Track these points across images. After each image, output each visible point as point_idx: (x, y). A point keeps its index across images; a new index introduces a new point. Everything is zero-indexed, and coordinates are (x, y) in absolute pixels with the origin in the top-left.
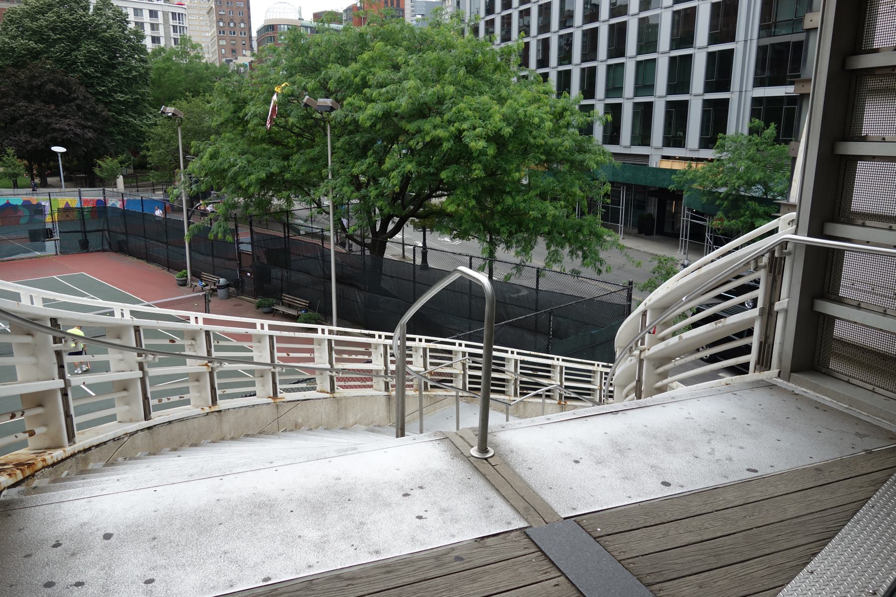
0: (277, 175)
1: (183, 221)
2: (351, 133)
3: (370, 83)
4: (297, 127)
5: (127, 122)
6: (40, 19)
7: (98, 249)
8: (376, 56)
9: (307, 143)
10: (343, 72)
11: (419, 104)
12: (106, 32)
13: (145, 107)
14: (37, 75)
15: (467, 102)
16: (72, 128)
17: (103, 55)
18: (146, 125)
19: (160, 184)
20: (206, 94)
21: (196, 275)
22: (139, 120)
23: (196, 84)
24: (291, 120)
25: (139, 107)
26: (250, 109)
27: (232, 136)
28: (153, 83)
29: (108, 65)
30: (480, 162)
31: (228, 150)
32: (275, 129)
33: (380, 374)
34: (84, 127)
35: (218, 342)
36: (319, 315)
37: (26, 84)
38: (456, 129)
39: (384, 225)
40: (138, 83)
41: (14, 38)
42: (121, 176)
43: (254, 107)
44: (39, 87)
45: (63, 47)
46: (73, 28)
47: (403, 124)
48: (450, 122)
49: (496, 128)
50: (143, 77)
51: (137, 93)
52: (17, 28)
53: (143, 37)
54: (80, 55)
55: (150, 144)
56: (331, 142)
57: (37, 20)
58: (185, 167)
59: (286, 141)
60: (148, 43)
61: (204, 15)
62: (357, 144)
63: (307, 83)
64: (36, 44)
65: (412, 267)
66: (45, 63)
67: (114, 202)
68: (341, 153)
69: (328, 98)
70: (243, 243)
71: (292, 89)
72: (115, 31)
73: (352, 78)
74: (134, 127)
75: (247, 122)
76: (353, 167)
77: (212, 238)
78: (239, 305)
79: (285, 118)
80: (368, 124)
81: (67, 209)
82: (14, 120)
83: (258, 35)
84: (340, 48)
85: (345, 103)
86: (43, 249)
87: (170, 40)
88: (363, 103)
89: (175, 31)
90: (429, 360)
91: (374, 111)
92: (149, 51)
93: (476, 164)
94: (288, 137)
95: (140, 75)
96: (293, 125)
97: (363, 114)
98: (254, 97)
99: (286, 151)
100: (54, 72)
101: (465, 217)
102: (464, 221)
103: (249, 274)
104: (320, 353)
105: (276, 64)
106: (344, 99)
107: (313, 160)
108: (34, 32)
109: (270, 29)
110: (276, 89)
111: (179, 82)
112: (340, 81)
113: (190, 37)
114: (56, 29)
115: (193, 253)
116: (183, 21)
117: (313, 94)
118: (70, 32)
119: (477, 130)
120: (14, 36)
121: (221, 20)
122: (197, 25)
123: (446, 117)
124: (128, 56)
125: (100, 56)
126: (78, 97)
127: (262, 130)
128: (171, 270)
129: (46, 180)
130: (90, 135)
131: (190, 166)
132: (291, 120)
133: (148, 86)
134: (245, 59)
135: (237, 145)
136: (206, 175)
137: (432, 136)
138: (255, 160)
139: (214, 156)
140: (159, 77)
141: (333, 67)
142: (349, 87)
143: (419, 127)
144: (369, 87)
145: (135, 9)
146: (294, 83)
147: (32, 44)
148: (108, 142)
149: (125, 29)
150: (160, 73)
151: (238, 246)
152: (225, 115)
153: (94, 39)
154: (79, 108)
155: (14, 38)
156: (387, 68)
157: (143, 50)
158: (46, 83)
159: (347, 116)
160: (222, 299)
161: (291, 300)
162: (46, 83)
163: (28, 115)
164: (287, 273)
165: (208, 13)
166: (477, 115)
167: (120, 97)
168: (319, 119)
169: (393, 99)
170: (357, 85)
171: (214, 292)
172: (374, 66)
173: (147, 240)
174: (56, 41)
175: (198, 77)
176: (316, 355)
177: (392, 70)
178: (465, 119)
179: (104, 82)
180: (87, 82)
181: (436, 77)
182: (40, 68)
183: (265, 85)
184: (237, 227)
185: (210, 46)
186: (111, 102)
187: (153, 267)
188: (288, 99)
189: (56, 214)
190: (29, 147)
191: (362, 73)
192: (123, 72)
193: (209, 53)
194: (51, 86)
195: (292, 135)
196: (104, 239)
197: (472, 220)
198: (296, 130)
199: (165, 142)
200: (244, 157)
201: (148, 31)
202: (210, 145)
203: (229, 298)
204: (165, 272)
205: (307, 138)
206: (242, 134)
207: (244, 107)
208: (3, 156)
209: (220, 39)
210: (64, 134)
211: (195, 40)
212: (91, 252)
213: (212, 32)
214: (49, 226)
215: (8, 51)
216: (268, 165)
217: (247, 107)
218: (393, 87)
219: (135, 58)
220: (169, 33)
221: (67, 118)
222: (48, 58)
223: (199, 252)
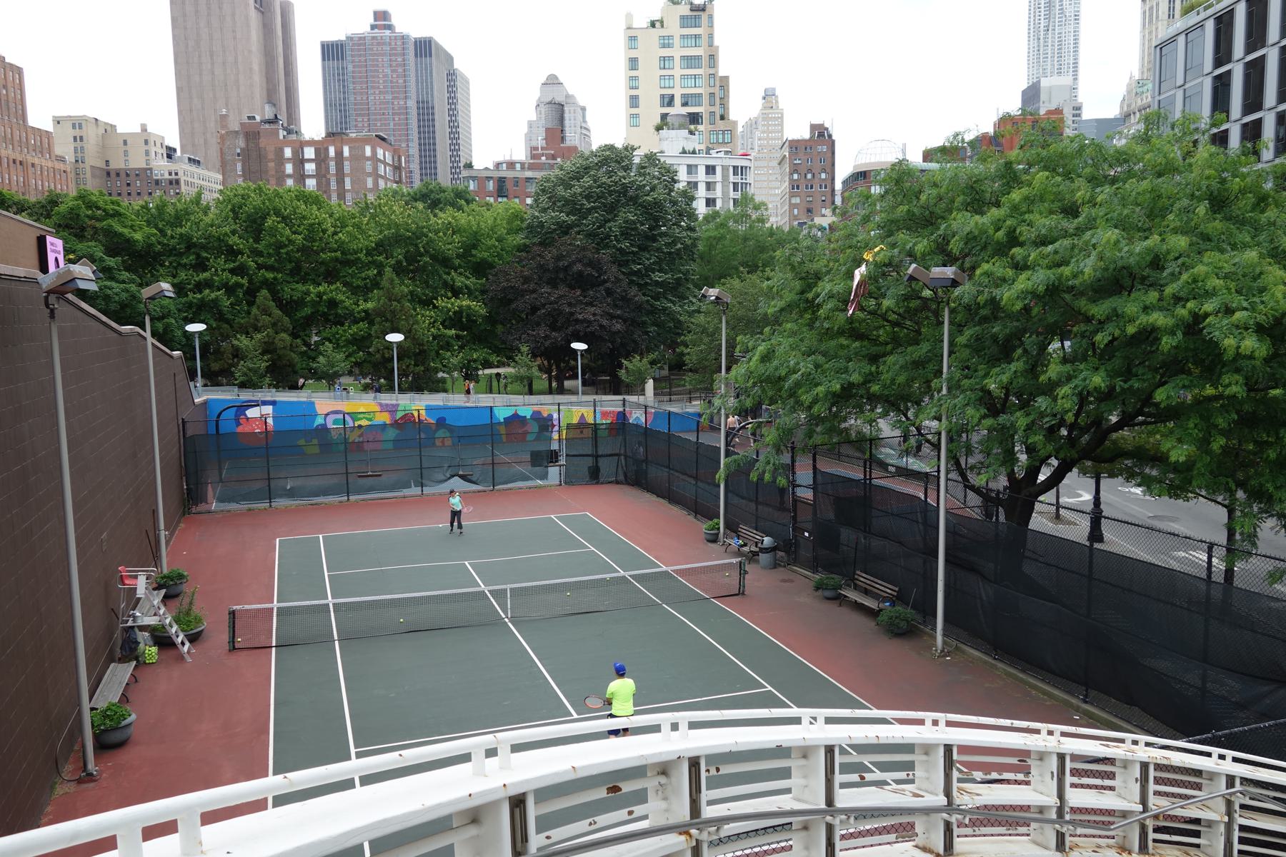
0: (859, 385)
1: (720, 448)
2: (985, 319)
3: (1022, 239)
4: (893, 312)
5: (665, 309)
6: (574, 186)
7: (610, 480)
8: (1035, 195)
9: (907, 335)
10: (977, 223)
11: (1114, 270)
12: (648, 195)
13: (688, 288)
14: (564, 253)
15: (1211, 263)
16: (598, 318)
17: (643, 224)
18: (687, 312)
19: (697, 390)
20: (767, 269)
21: (732, 527)
22: (680, 306)
23: (756, 256)
24: (887, 303)
25: (681, 289)
26: (825, 287)
27: (796, 328)
28: (702, 258)
29: (647, 237)
30: (1238, 371)
31: (788, 348)
32: (860, 314)
33: (1047, 816)
34: (612, 317)
35: (718, 770)
36: (913, 612)
37: (551, 266)
38: (1190, 312)
39: (1033, 471)
40: (681, 258)
41: (544, 210)
42: (651, 381)
43: (831, 284)
44: (566, 269)
45: (597, 217)
46: (610, 193)
47: (1082, 304)
48: (1178, 299)
49: (1276, 311)
50: (690, 249)
51: (680, 271)
52: (549, 198)
53: (693, 199)
54: (615, 227)
55: (689, 338)
56: (950, 335)
57: (571, 187)
58: (728, 369)
59: (875, 333)
60: (700, 208)
61: (774, 168)
62: (995, 338)
63: (915, 244)
64: (567, 216)
65: (1087, 551)
66: (575, 239)
67: (636, 416)
68: (966, 353)
69: (945, 265)
70: (801, 486)
71: (890, 254)
72: (660, 194)
73: (991, 232)
74: (671, 316)
75: (819, 306)
76: (986, 375)
77: (755, 479)
78: (791, 581)
79: (876, 298)
80: (1019, 306)
81: (582, 425)
82: (534, 309)
83: (843, 187)
84: (972, 187)
85: (978, 272)
86: (544, 476)
87: (729, 202)
88: (1010, 273)
89: (735, 189)
90: (1152, 787)
91: (1030, 283)
92: (701, 217)
93: (1228, 375)
94: (878, 328)
95: (686, 247)
96: (889, 309)
97: (1009, 289)
98: (831, 269)
99: (874, 350)
100: (584, 249)
101: (1199, 465)
102: (1195, 472)
103: (806, 534)
104: (927, 771)
105: (866, 220)
106: (973, 268)
107: (918, 364)
108: (567, 202)
109: (861, 176)
110: (865, 257)
111: (734, 254)
112: (970, 238)
113: (753, 195)
114: (592, 197)
115: (730, 495)
116: (746, 175)
117: (924, 261)
118: (606, 199)
119: (1238, 315)
120: (545, 209)
121: (796, 171)
122: (765, 181)
123: (1169, 290)
124: (673, 225)
125: (638, 225)
126: (608, 278)
127: (841, 318)
128: (699, 516)
129: (563, 383)
130: (618, 326)
131: (733, 372)
132: (887, 303)
133: (695, 261)
134: (825, 219)
135: (802, 340)
136: (755, 384)
137: (1140, 324)
138: (827, 363)
139: (766, 358)
140: (710, 250)
141: (960, 216)
142: (984, 248)
143: (1115, 310)
144: (1021, 245)
145: (689, 166)
146: (893, 246)
147: (563, 216)
148: (639, 336)
149: (671, 190)
150: (711, 245)
151: (793, 490)
152: (789, 297)
153: (634, 205)
154: (609, 292)
155: (544, 210)
156: (1051, 212)
157: (692, 215)
158: (574, 263)
159: (980, 293)
160: (764, 568)
161: (868, 582)
162: (574, 263)
163: (550, 304)
164: (865, 539)
165: (779, 164)
166: (1232, 285)
167: (658, 277)
168: (928, 299)
169: (1067, 263)
170: (998, 243)
171: (754, 555)
172: (1031, 212)
173: (672, 472)
174: (589, 211)
175: (759, 246)
176: (919, 773)
177: (1062, 215)
178: (1209, 294)
179: (641, 259)
180: (622, 260)
181: (1143, 221)
182: (570, 245)
183: (849, 251)
184: (793, 461)
185: (779, 206)
186: (646, 283)
187: (676, 511)
188: (884, 269)
189: (564, 432)
190: (547, 343)
191: (1008, 223)
192: (665, 245)
193: (777, 216)
194: (578, 267)
195: (886, 323)
196: (620, 469)
197: (1211, 472)
198: (893, 317)
199: (708, 335)
200: (810, 358)
201: (702, 192)
202: (763, 341)
203: (775, 568)
204: (691, 518)
205: (908, 329)
206: (811, 325)
207: (816, 284)
208: (517, 356)
209: (792, 195)
210: (588, 327)
211: (758, 199)
212: (602, 483)
213: (783, 188)
214: (555, 446)
215: (537, 226)
216: (846, 371)
217: (820, 284)
218: (1066, 242)
219: (681, 226)
220: (728, 192)
221: (594, 306)
222: (578, 233)
223: (737, 495)
